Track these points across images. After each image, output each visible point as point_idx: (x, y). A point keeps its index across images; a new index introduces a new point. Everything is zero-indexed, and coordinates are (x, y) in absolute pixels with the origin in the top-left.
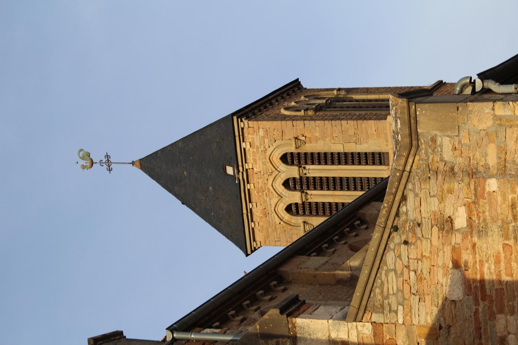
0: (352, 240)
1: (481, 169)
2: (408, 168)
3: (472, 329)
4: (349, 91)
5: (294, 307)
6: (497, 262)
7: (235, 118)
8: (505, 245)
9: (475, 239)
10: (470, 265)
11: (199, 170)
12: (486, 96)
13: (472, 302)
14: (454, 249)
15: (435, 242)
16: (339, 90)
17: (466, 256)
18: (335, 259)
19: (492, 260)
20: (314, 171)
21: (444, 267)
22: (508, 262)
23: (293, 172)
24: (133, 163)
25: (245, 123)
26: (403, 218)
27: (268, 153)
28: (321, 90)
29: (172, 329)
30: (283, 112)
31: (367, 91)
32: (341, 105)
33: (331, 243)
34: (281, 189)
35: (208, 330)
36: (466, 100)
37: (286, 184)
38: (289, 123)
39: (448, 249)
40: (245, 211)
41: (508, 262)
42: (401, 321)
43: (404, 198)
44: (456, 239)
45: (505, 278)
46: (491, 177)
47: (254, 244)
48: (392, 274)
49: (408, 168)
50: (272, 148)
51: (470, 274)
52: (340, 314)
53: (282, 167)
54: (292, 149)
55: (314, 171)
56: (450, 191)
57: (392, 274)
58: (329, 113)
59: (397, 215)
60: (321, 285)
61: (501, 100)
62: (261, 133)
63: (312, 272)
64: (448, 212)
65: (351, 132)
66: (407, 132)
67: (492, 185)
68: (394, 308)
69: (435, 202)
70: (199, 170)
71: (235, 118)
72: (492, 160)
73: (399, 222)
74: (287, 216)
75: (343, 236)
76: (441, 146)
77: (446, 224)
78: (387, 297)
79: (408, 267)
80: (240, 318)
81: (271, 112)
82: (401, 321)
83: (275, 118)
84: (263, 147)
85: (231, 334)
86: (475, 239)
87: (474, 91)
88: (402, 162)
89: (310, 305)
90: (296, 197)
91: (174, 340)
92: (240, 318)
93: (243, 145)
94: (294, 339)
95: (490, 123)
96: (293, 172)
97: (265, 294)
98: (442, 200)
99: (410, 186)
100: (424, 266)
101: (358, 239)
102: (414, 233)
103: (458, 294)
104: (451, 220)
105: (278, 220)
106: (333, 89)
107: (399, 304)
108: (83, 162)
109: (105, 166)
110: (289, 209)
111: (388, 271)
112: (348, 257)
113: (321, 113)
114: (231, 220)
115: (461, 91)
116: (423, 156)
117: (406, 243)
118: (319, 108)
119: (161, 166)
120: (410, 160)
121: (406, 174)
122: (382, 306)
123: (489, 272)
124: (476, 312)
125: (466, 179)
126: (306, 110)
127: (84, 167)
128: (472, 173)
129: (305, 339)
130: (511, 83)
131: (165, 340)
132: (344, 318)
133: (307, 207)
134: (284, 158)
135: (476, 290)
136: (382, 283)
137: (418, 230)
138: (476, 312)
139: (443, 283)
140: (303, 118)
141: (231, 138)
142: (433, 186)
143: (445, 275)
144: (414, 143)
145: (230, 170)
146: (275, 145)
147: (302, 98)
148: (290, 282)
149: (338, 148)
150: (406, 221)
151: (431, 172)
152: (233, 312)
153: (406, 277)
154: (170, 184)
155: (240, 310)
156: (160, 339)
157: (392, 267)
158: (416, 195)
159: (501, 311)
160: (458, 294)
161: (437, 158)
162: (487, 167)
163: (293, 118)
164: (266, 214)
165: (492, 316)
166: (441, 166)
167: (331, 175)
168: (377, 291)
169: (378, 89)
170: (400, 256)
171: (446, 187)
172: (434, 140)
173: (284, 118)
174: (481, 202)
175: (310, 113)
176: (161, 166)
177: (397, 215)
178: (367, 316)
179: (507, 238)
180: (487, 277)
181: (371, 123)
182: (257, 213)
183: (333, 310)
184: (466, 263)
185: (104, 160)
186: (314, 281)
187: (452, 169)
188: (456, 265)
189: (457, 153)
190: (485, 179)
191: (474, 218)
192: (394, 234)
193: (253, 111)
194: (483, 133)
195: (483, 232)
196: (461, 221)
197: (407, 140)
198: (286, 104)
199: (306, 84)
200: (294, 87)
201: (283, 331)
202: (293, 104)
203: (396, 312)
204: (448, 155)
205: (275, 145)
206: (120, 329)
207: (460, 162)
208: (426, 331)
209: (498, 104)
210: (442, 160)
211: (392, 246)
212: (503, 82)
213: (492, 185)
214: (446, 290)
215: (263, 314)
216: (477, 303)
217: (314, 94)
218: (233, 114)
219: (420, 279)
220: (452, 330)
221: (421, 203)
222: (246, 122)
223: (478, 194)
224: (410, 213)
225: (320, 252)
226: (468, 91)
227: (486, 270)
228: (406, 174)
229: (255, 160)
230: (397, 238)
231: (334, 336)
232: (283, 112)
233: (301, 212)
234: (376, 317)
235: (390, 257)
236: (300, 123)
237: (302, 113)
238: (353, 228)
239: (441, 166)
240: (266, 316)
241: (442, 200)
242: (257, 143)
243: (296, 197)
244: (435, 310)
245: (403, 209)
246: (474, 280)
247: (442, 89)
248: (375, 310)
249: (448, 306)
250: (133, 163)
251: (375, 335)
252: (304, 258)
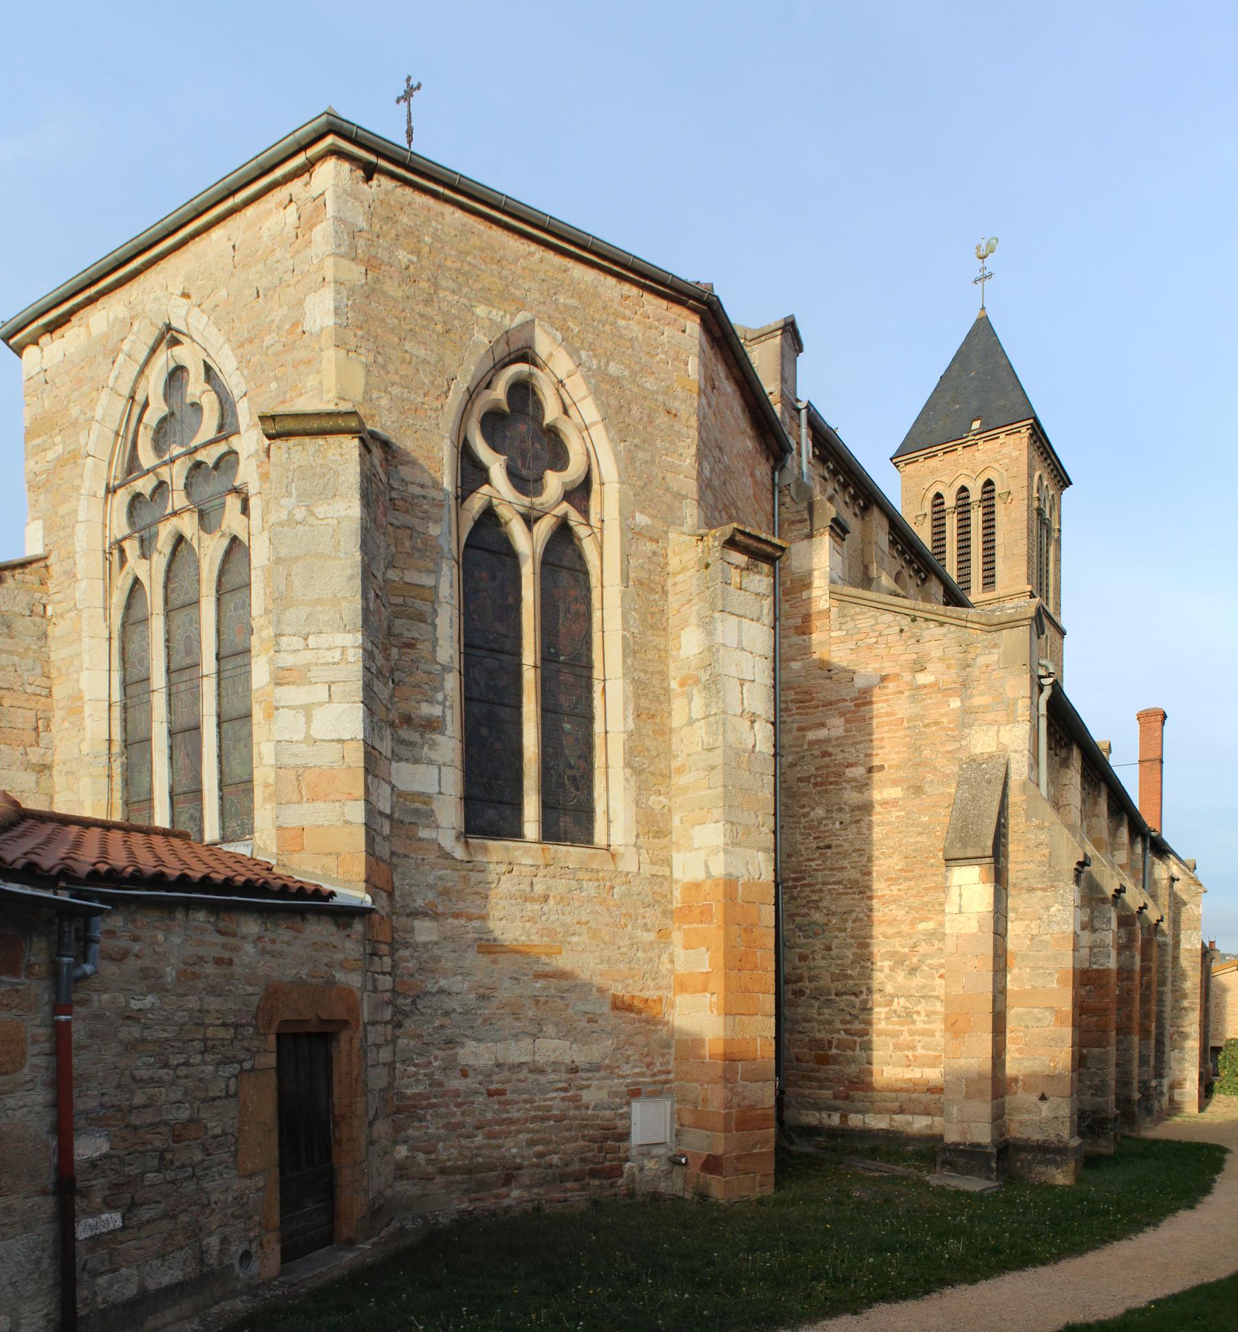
0: (907, 572)
1: (969, 692)
2: (969, 625)
3: (832, 698)
4: (1058, 541)
5: (839, 529)
6: (888, 714)
7: (1031, 421)
8: (903, 719)
9: (907, 693)
10: (885, 691)
11: (979, 390)
12: (1036, 689)
13: (853, 696)
14: (898, 675)
15: (903, 658)
16: (1059, 531)
17: (891, 686)
18: (887, 559)
19: (890, 709)
20: (977, 517)
21: (882, 668)
22: (888, 724)
23: (975, 495)
24: (983, 308)
25: (1025, 433)
26: (924, 625)
27: (994, 465)
28: (1060, 511)
29: (809, 406)
30: (1037, 474)
31: (1058, 560)
32: (1044, 529)
33: (902, 553)
34: (958, 485)
35: (810, 444)
36: (1032, 670)
37: (963, 489)
38: (1025, 483)
39: (897, 670)
40: (935, 449)
41: (888, 724)
42: (833, 634)
43: (942, 624)
44: (907, 677)
45: (875, 722)
46: (962, 701)
47: (902, 464)
48: (873, 621)
49: (969, 625)
50: (999, 468)
51: (877, 691)
52: (835, 577)
53: (981, 482)
54: (999, 489)
55: (977, 517)
56: (948, 666)
57: (873, 621)
58: (1035, 524)
59: (926, 620)
60: (862, 550)
61: (1032, 703)
62: (1015, 454)
63: (874, 539)
64: (930, 667)
65: (1015, 550)
66: (1003, 620)
67: (955, 703)
68: (844, 627)
69: (939, 653)
70: (979, 390)
71: (1031, 421)
72: (978, 701)
73: (920, 622)
74: (931, 495)
75: (910, 563)
76: (990, 653)
77: (919, 666)
78: (853, 620)
79: (880, 635)
80: (827, 475)
81: (1037, 460)
82: (833, 634)
83: (1031, 467)
84: (1002, 458)
85: (809, 471)
86: (907, 693)
87: (1041, 677)
88: (975, 619)
89: (841, 546)
90: (950, 501)
91: (799, 411)
92: (827, 475)
93: (1002, 436)
94: (810, 536)
95: (1011, 696)
96: (975, 495)
97: (850, 496)
98: (941, 659)
99: (953, 628)
100: (881, 650)
101: (907, 578)
102: (910, 638)
103: (859, 683)
104: (923, 669)
105: (926, 487)
106: (1060, 524)
107: (847, 631)
108: (984, 246)
109: (979, 275)
110: (938, 496)
111: (875, 617)
112: (889, 574)
113: (1035, 515)
114: (928, 436)
115: (1042, 666)
116: (980, 638)
117: (902, 631)
118: (1040, 512)
119: (981, 347)
120: (976, 626)
121: (964, 623)
122: (845, 616)
123: (879, 707)
124: (845, 700)
125: (959, 680)
126: (1039, 499)
127: (978, 248)
128: (964, 685)
129: (811, 546)
130: (1048, 710)
131: (798, 400)
132: (832, 582)
133: (941, 515)
134: (989, 483)
135: (864, 699)
136: (864, 613)
137: (913, 641)
138: (845, 700)
139: (867, 669)
140: (1030, 497)
141: (1010, 420)
142: (954, 650)
143: (875, 669)
144: (993, 628)
145: (976, 425)
146: (1002, 471)
147: (1051, 492)
148: (863, 519)
149: (999, 538)
150: (921, 629)
151: (966, 647)
152: (831, 467)
153: (871, 634)
154: (961, 358)
155: (834, 473)
156: (799, 397)
157: (880, 620)
158: (945, 635)
159: (847, 721)
160: (859, 683)
161: (978, 651)
162: (970, 697)
163: (1030, 486)
164: (932, 473)
165: (842, 714)
166: (972, 655)
167: (973, 535)
168: (858, 610)
169: (1060, 571)
170: (889, 626)
171: (953, 662)
172: (995, 646)
173: (1031, 476)
174: (940, 695)
175: (1036, 504)
176: (981, 347)
177: (926, 620)
178: (836, 603)
179: (909, 720)
180: (875, 706)
181: (1024, 570)
182: (933, 463)
183: (839, 570)
184: (886, 687)
185: (986, 273)
186: (866, 541)
187: (969, 666)
188: (884, 679)
189: (984, 669)
190: (960, 696)
191: (925, 690)
192: (909, 619)
193: (1039, 438)
194: (1001, 690)
195: (914, 699)
196: (922, 679)
197: (995, 621)
198: (1045, 475)
199: (1067, 492)
200: (1063, 480)
201: (817, 525)
202: (1045, 483)
203: (840, 629)
204: (982, 660)
205: (1002, 471)
206: (805, 348)
207: (975, 672)
208: (826, 658)
209: (1028, 701)
210: (977, 655)
211: (899, 617)
212: (1050, 703)
213: (955, 703)
214: (861, 670)
215: (831, 499)
216: (853, 700)
217: (1056, 504)
218: (1035, 419)
219: (870, 647)
220: (828, 681)
221: (939, 639)
222: (1027, 434)
223: (946, 692)
224: (928, 632)
225: (893, 543)
226: (1042, 672)
227: (880, 705)
228: (964, 623)
229: (986, 451)
230: (905, 622)
231: (816, 573)
232: (1037, 474)
233: (936, 509)
234: (834, 610)
235: (888, 617)
236: (1025, 494)
237: (1036, 495)
238: (918, 571)
239: (972, 655)
240: (828, 504)
241: (941, 659)
242: (1005, 451)
243: (950, 501)
244: (845, 664)
245: (932, 625)
246: (871, 696)
247: (1058, 636)
248: (841, 609)
249: (850, 675)
250: (983, 308)
251: (819, 612)
252: (887, 528)
